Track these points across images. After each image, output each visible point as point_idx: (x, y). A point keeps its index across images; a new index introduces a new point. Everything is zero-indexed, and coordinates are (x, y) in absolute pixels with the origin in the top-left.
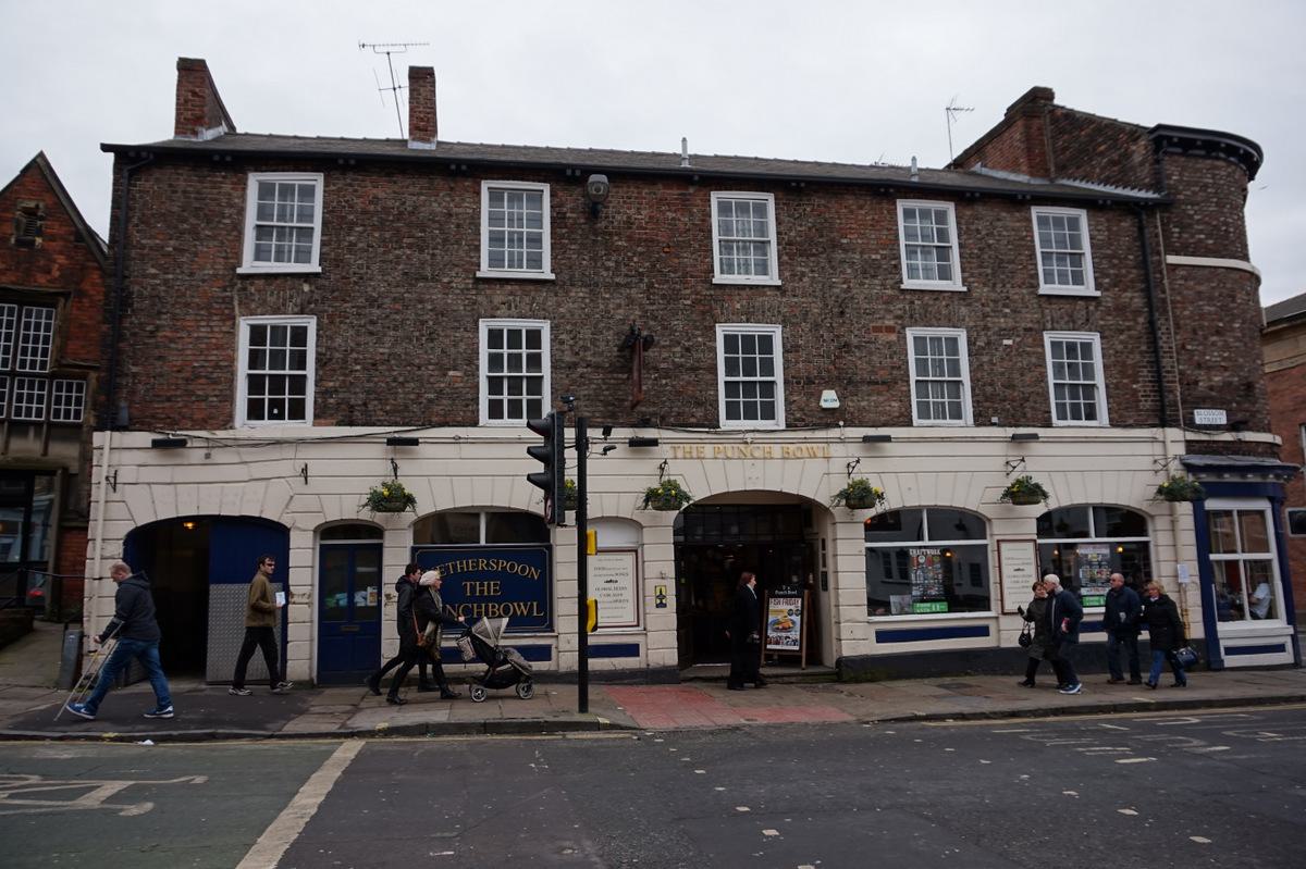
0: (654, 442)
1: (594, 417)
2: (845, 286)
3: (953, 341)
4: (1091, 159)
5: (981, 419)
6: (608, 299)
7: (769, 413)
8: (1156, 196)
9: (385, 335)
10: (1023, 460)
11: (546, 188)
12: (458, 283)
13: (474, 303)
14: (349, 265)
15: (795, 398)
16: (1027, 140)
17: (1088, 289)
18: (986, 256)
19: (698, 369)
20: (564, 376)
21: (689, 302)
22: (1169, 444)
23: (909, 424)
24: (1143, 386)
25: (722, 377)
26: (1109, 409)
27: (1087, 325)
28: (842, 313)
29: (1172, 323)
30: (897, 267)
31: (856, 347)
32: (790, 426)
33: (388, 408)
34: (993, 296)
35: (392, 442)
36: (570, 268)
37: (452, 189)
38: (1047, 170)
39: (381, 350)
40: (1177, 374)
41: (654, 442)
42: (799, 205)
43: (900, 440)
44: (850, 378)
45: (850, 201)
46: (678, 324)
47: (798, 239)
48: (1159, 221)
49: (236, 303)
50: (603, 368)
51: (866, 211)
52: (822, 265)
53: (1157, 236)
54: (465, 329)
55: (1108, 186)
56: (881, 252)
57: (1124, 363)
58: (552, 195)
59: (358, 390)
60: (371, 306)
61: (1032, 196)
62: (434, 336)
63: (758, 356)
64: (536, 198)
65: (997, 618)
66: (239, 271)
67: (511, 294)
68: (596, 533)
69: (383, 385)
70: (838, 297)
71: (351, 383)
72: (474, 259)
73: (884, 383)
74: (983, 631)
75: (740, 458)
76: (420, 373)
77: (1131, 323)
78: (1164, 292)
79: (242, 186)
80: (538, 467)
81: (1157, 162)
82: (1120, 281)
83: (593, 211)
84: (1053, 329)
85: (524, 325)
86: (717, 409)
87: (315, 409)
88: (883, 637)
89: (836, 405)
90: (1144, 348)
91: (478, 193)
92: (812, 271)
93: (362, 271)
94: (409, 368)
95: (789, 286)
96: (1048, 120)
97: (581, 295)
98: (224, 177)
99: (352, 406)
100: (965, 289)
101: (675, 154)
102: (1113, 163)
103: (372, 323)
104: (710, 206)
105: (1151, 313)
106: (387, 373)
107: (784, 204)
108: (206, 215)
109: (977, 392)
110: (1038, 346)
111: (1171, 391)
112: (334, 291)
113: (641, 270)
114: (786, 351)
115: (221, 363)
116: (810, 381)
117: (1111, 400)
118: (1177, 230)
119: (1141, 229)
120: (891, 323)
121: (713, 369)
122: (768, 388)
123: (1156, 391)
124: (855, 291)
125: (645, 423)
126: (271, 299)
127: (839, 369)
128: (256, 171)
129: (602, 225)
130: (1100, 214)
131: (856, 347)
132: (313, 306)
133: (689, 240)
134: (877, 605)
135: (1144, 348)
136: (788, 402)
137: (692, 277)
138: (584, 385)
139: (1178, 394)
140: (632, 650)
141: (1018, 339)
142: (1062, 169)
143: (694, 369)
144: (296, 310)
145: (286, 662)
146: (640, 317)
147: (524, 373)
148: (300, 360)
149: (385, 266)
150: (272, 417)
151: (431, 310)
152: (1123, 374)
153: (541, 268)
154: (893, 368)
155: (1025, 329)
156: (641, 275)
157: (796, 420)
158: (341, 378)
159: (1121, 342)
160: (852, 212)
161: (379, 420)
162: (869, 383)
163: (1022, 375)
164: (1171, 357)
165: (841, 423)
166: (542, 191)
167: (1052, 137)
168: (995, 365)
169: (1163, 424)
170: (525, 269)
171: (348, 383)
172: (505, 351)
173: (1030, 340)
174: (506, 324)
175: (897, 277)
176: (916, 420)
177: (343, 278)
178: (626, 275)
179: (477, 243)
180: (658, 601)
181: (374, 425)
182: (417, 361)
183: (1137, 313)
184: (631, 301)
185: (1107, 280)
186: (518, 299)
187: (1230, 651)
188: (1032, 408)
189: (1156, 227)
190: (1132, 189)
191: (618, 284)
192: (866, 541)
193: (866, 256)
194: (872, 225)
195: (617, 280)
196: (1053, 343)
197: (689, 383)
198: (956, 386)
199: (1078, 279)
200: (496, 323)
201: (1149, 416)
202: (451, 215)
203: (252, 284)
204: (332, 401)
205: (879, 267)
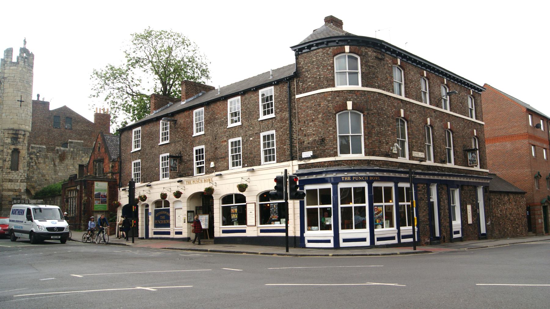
27: (272, 128)
28: (216, 138)
45: (218, 104)
48: (295, 82)
53: (294, 88)
57: (282, 139)
74: (244, 231)
84: (263, 132)
130: (277, 86)
141: (254, 137)
155: (256, 134)
185: (278, 110)
187: (309, 241)
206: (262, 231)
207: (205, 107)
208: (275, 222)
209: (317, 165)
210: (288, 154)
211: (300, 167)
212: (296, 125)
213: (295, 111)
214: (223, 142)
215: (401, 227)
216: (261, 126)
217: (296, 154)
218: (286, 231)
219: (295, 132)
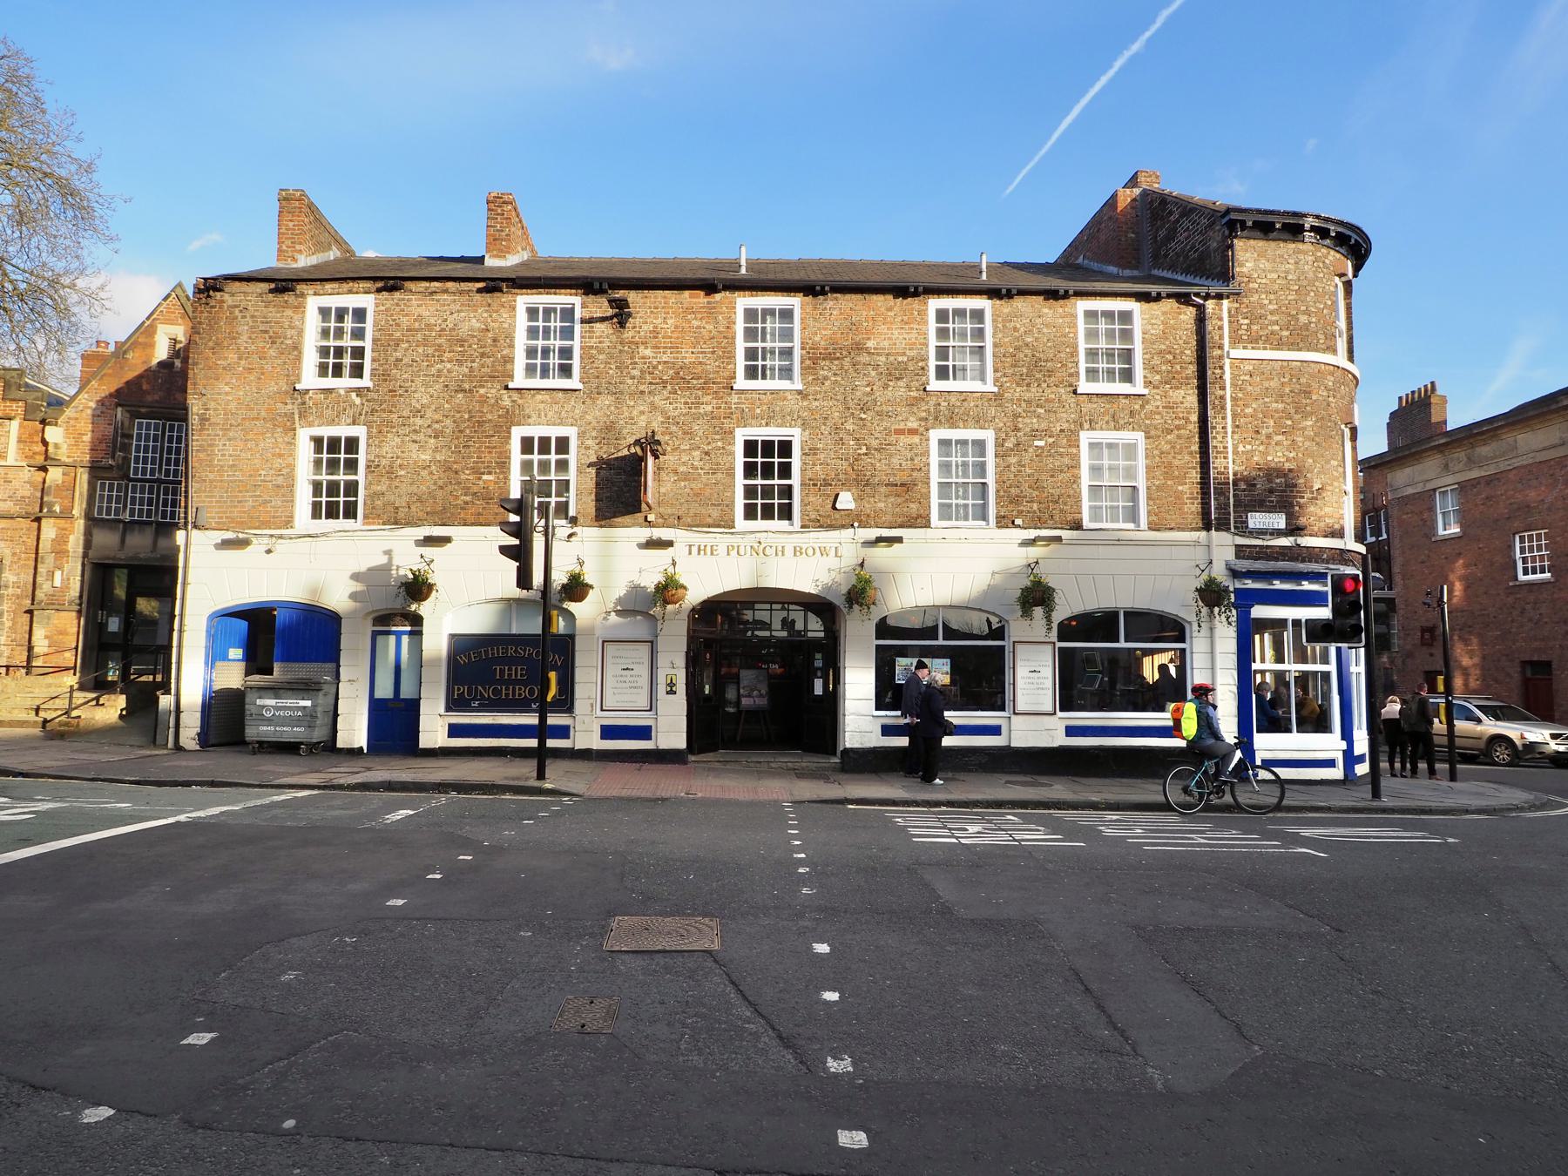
2: (868, 389)
18: (1022, 355)
26: (1149, 512)
31: (876, 449)
49: (296, 417)
53: (1221, 328)
74: (995, 730)
89: (852, 506)
93: (406, 385)
97: (607, 402)
103: (415, 431)
109: (1002, 493)
110: (1074, 446)
117: (1151, 503)
121: (730, 473)
131: (876, 449)
137: (714, 383)
140: (644, 732)
141: (1051, 440)
152: (1167, 475)
154: (913, 470)
156: (665, 382)
175: (924, 378)
180: (669, 689)
191: (642, 392)
193: (892, 358)
202: (488, 330)
206: (1071, 731)
209: (1299, 555)
210: (1193, 509)
211: (1240, 551)
212: (1226, 433)
213: (1222, 393)
214: (899, 432)
215: (548, 740)
219: (1221, 452)
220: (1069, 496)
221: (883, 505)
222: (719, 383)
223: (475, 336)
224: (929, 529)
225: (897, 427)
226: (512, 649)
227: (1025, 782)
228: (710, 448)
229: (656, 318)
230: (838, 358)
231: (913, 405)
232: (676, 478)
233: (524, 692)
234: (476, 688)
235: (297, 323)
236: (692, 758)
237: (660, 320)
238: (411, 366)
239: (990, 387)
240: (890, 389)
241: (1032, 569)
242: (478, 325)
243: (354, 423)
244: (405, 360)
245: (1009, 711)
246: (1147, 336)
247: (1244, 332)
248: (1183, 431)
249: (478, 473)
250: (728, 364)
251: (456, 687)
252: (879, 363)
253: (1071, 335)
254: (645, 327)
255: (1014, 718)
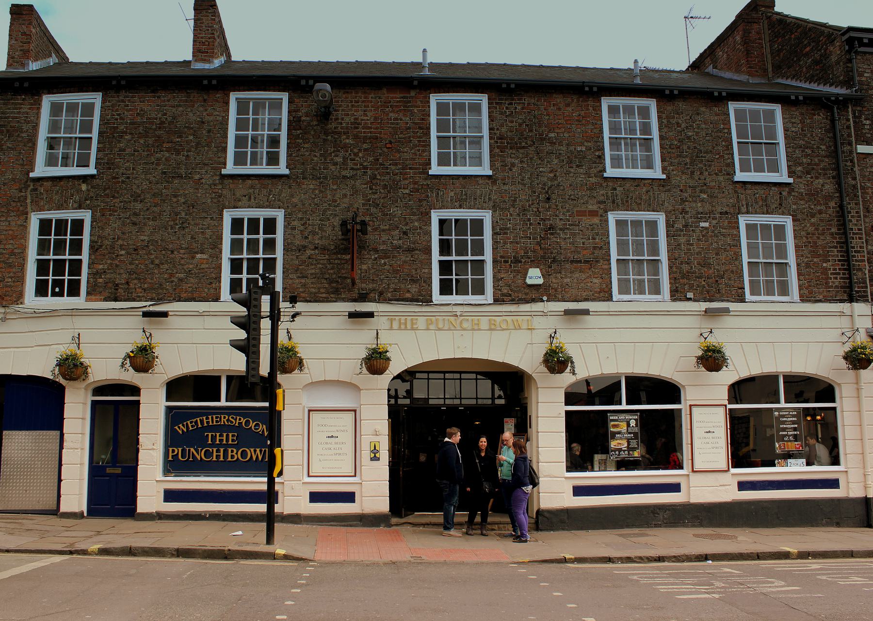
0: (370, 315)
1: (319, 292)
2: (552, 175)
3: (652, 226)
4: (799, 60)
5: (677, 294)
6: (336, 190)
7: (479, 289)
8: (848, 92)
9: (145, 224)
10: (711, 332)
11: (285, 97)
12: (207, 180)
13: (220, 196)
14: (119, 167)
15: (502, 276)
16: (745, 43)
17: (783, 177)
18: (685, 147)
19: (414, 250)
20: (294, 257)
21: (407, 191)
22: (856, 318)
23: (609, 298)
24: (833, 265)
25: (436, 256)
26: (800, 286)
27: (781, 209)
28: (548, 199)
29: (861, 207)
30: (601, 158)
31: (561, 229)
32: (497, 301)
33: (146, 286)
34: (692, 183)
35: (146, 314)
36: (303, 164)
37: (205, 101)
38: (765, 70)
39: (142, 238)
40: (866, 254)
41: (370, 315)
42: (511, 104)
43: (598, 313)
44: (554, 258)
45: (559, 99)
46: (396, 211)
47: (509, 134)
48: (850, 113)
49: (29, 201)
50: (328, 250)
51: (571, 108)
52: (531, 156)
54: (212, 218)
55: (812, 84)
56: (586, 144)
57: (815, 243)
58: (290, 102)
59: (122, 271)
60: (135, 201)
61: (680, 91)
62: (185, 225)
63: (469, 238)
64: (276, 105)
65: (688, 475)
66: (32, 175)
67: (252, 187)
68: (865, 397)
69: (142, 267)
70: (544, 184)
71: (117, 266)
72: (222, 159)
73: (586, 262)
74: (675, 488)
75: (449, 330)
76: (173, 256)
77: (823, 207)
78: (854, 179)
79: (38, 105)
80: (241, 335)
81: (850, 61)
82: (813, 169)
83: (325, 114)
84: (748, 212)
85: (262, 214)
86: (430, 285)
87: (87, 288)
88: (579, 491)
89: (540, 281)
90: (834, 230)
91: (227, 103)
92: (522, 162)
93: (129, 172)
94: (164, 252)
95: (500, 176)
96: (766, 26)
97: (312, 186)
98: (24, 99)
99: (117, 285)
100: (664, 177)
101: (413, 64)
102: (816, 62)
103: (135, 214)
104: (429, 107)
105: (841, 198)
106: (146, 257)
107: (497, 103)
108: (8, 131)
109: (674, 269)
110: (734, 228)
111: (860, 270)
112: (105, 190)
113: (365, 164)
114: (495, 234)
115: (16, 251)
116: (517, 261)
117: (802, 278)
118: (868, 122)
119: (833, 121)
120: (595, 208)
121: (428, 251)
122: (479, 266)
123: (844, 269)
124: (560, 179)
125: (363, 298)
126: (56, 198)
127: (545, 248)
128: (49, 93)
129: (332, 126)
130: (794, 109)
131: (561, 229)
132: (88, 202)
133: (410, 137)
134: (576, 463)
135: (834, 230)
136: (496, 279)
137: (410, 168)
138: (312, 265)
139: (867, 272)
140: (349, 497)
141: (714, 222)
142: (778, 69)
143: (410, 250)
144: (76, 205)
145: (61, 496)
146: (364, 205)
147: (261, 255)
148: (77, 247)
149: (147, 166)
150: (54, 294)
151: (184, 203)
152: (814, 254)
153: (278, 165)
154: (595, 248)
155: (721, 213)
156: (365, 168)
157: (503, 295)
158: (109, 262)
159: (812, 225)
160: (559, 109)
161: (139, 297)
162: (572, 262)
163: (717, 254)
164: (860, 238)
165: (545, 298)
166: (282, 99)
167: (770, 41)
168: (692, 245)
169: (851, 300)
170: (248, 166)
171: (114, 266)
172: (245, 237)
173: (726, 223)
174: (246, 214)
175: (601, 166)
176: (748, 296)
177: (115, 178)
178: (352, 169)
179: (223, 145)
180: (373, 455)
181: (134, 300)
182: (171, 246)
183: (829, 198)
184: (355, 192)
185: (800, 168)
186: (257, 191)
188: (726, 284)
189: (848, 120)
190: (831, 85)
191: (344, 177)
192: (566, 404)
193: (572, 148)
194: (578, 121)
195: (344, 173)
196: (747, 225)
197: (405, 262)
198: (655, 264)
199: (649, 166)
200: (239, 213)
201: (838, 292)
202: (203, 123)
203: (41, 186)
204: (101, 280)
205: (584, 157)
206: (743, 486)
207: (494, 95)
208: (789, 461)
212: (859, 217)
214: (582, 213)
216: (742, 197)
217: (862, 287)
218: (270, 496)
220: (732, 271)
221: (568, 280)
222: (416, 169)
223: (192, 128)
224: (611, 303)
225: (579, 209)
226: (225, 417)
227: (707, 535)
228: (408, 228)
229: (356, 111)
230: (524, 147)
231: (592, 189)
232: (376, 256)
233: (237, 453)
234: (189, 450)
235: (32, 118)
236: (394, 520)
237: (361, 113)
238: (133, 155)
239: (657, 173)
240: (572, 175)
241: (706, 338)
242: (194, 118)
243: (80, 207)
244: (128, 151)
245: (688, 469)
246: (788, 133)
247: (867, 131)
248: (824, 215)
249: (192, 254)
250: (424, 151)
251: (171, 449)
252: (562, 152)
253: (726, 131)
254: (347, 119)
255: (693, 477)
